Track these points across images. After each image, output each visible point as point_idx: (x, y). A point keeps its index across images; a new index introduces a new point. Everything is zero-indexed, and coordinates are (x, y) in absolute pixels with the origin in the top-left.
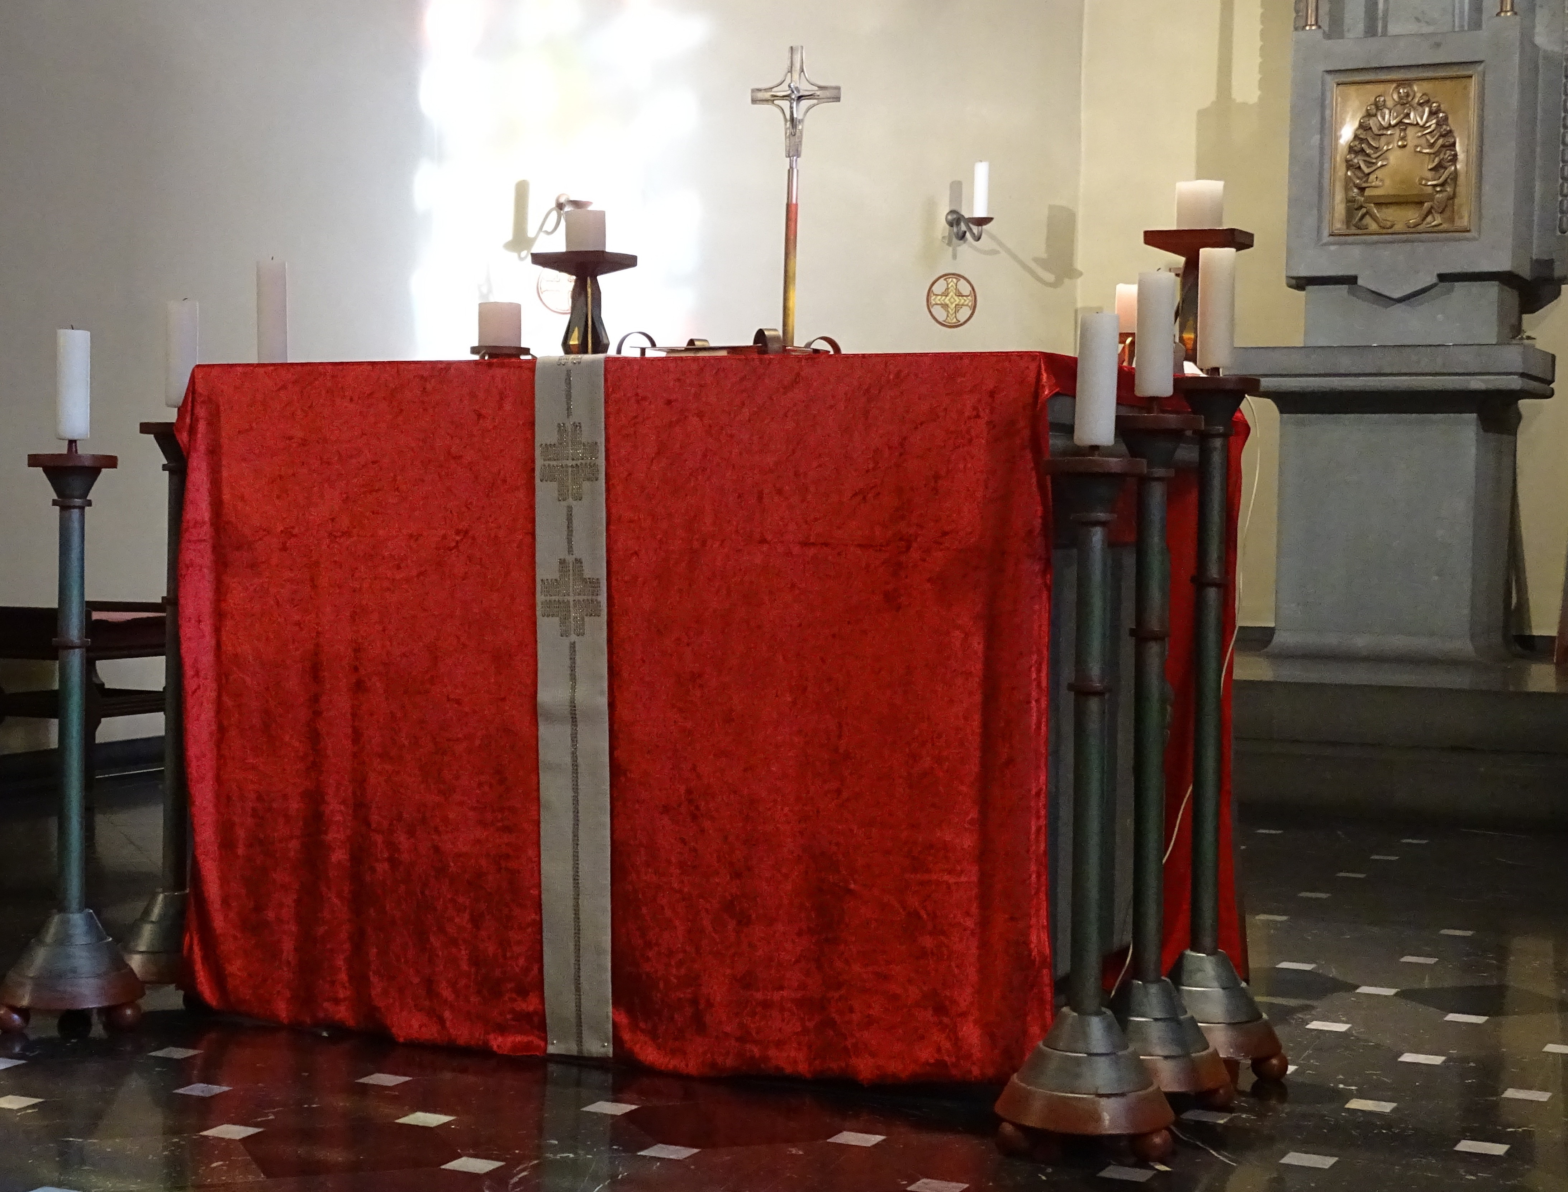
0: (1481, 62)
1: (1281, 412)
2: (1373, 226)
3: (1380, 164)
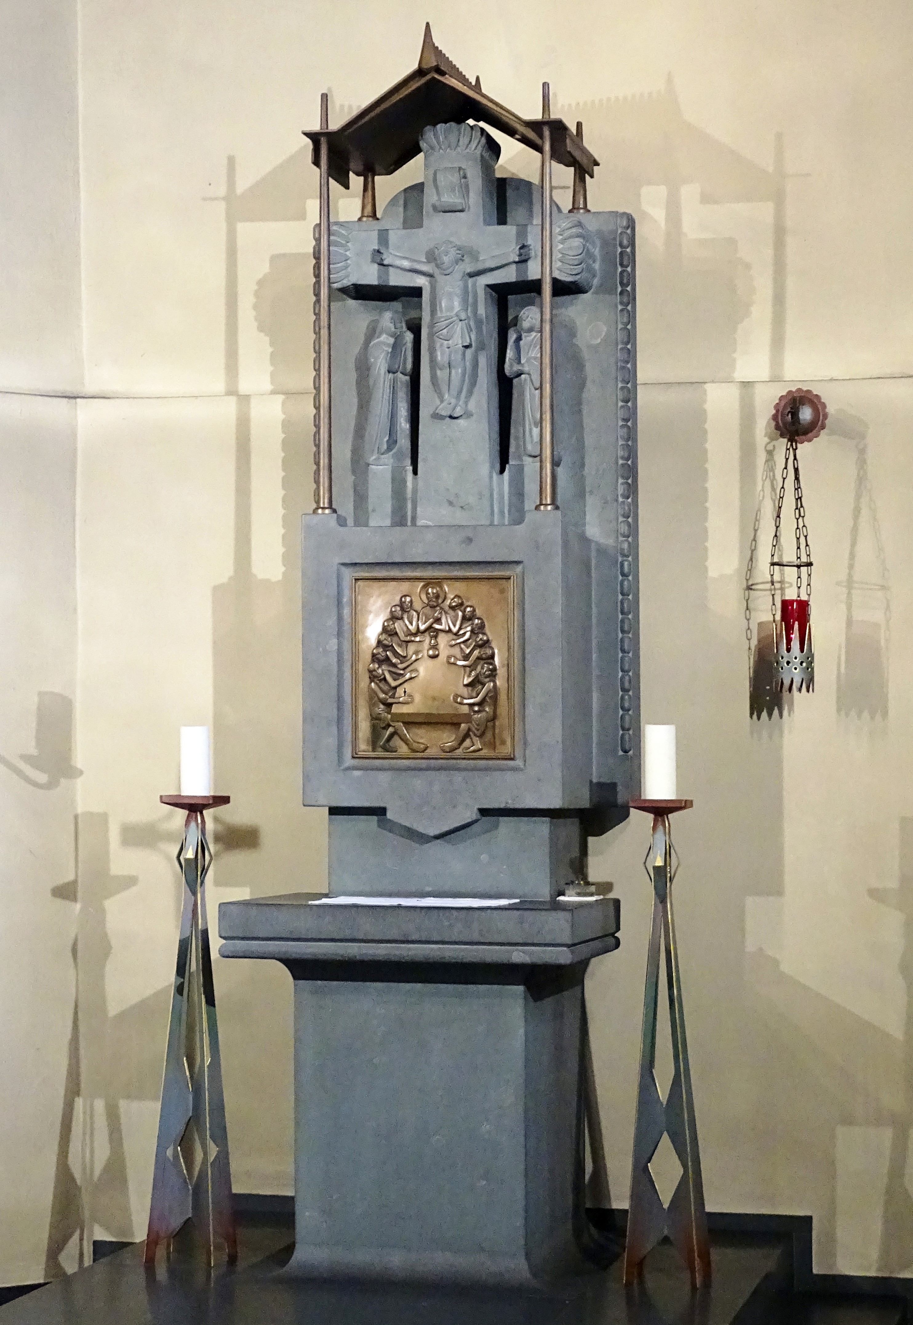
0: (518, 563)
1: (295, 977)
2: (403, 749)
3: (408, 676)
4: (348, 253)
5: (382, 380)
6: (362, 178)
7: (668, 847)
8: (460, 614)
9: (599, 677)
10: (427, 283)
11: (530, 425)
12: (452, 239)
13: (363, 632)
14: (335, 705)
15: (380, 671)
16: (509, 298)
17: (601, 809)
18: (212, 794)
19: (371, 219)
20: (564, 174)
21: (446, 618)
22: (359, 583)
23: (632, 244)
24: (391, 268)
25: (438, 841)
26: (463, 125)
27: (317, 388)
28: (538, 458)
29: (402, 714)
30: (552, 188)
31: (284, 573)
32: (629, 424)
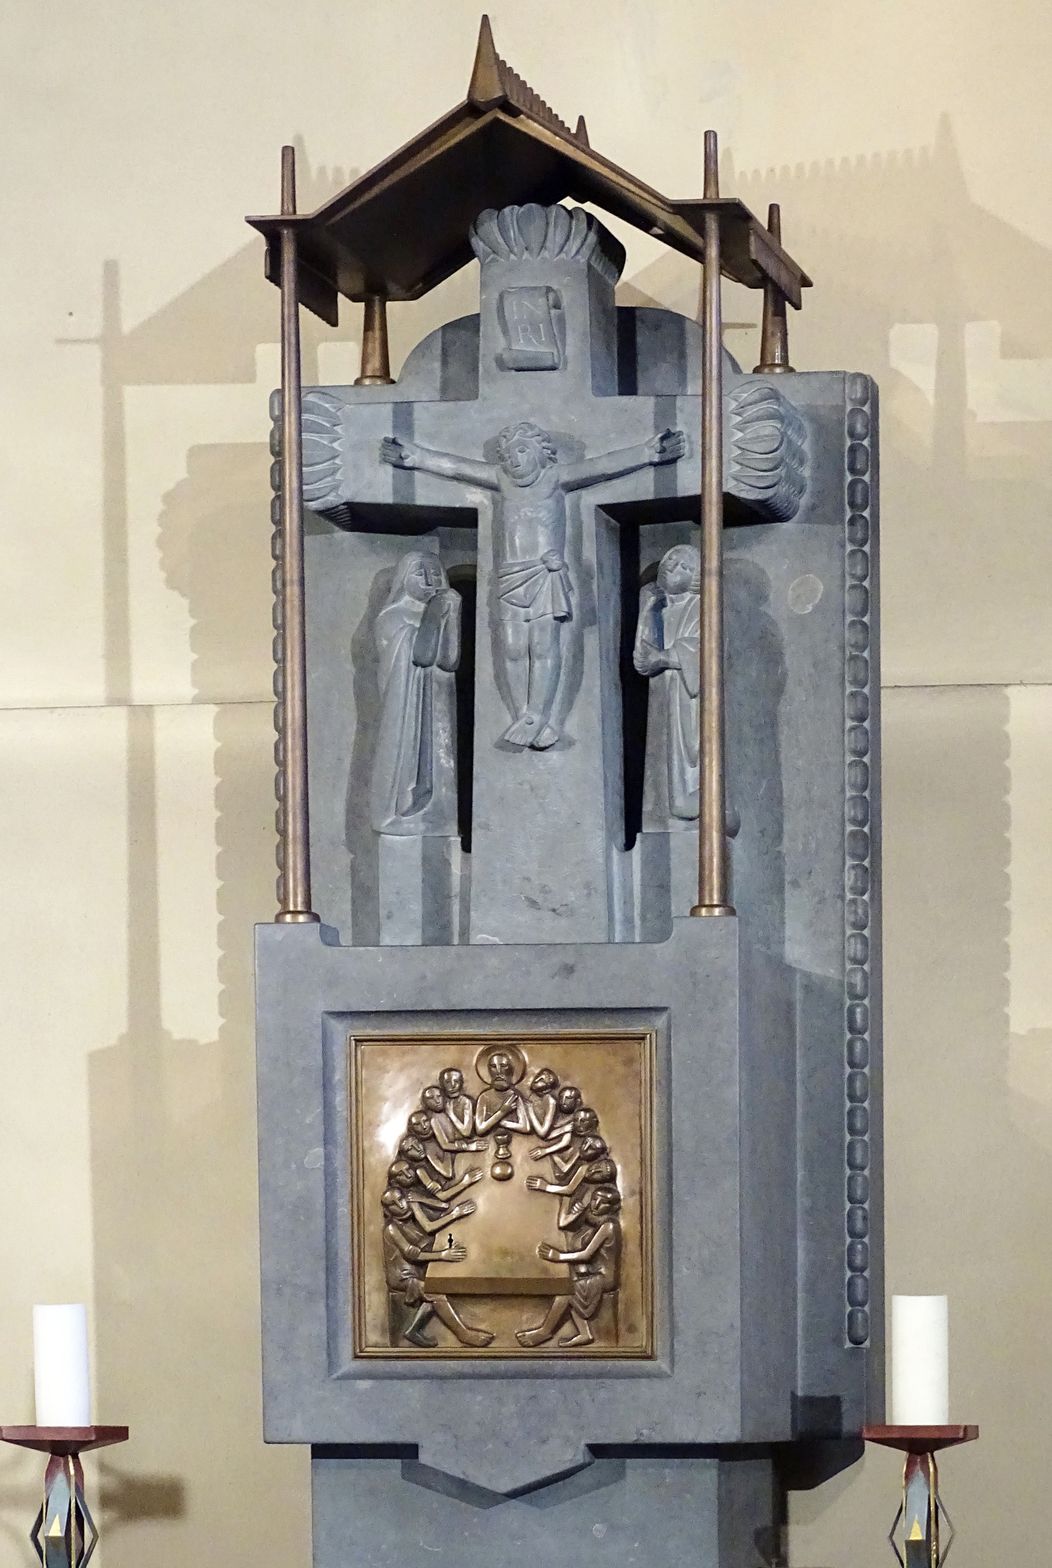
0: (665, 1009)
2: (449, 1342)
3: (456, 1213)
4: (335, 445)
5: (403, 678)
6: (362, 305)
7: (932, 1508)
8: (552, 1101)
9: (810, 1212)
10: (486, 502)
11: (681, 760)
12: (532, 420)
13: (372, 1135)
14: (323, 1263)
15: (404, 1204)
16: (640, 528)
17: (814, 1442)
18: (95, 1423)
19: (379, 382)
20: (745, 302)
21: (527, 1110)
22: (363, 1047)
23: (873, 430)
24: (416, 473)
25: (513, 1502)
26: (553, 209)
27: (281, 694)
28: (697, 822)
29: (447, 1280)
30: (721, 326)
31: (222, 1029)
32: (866, 759)
